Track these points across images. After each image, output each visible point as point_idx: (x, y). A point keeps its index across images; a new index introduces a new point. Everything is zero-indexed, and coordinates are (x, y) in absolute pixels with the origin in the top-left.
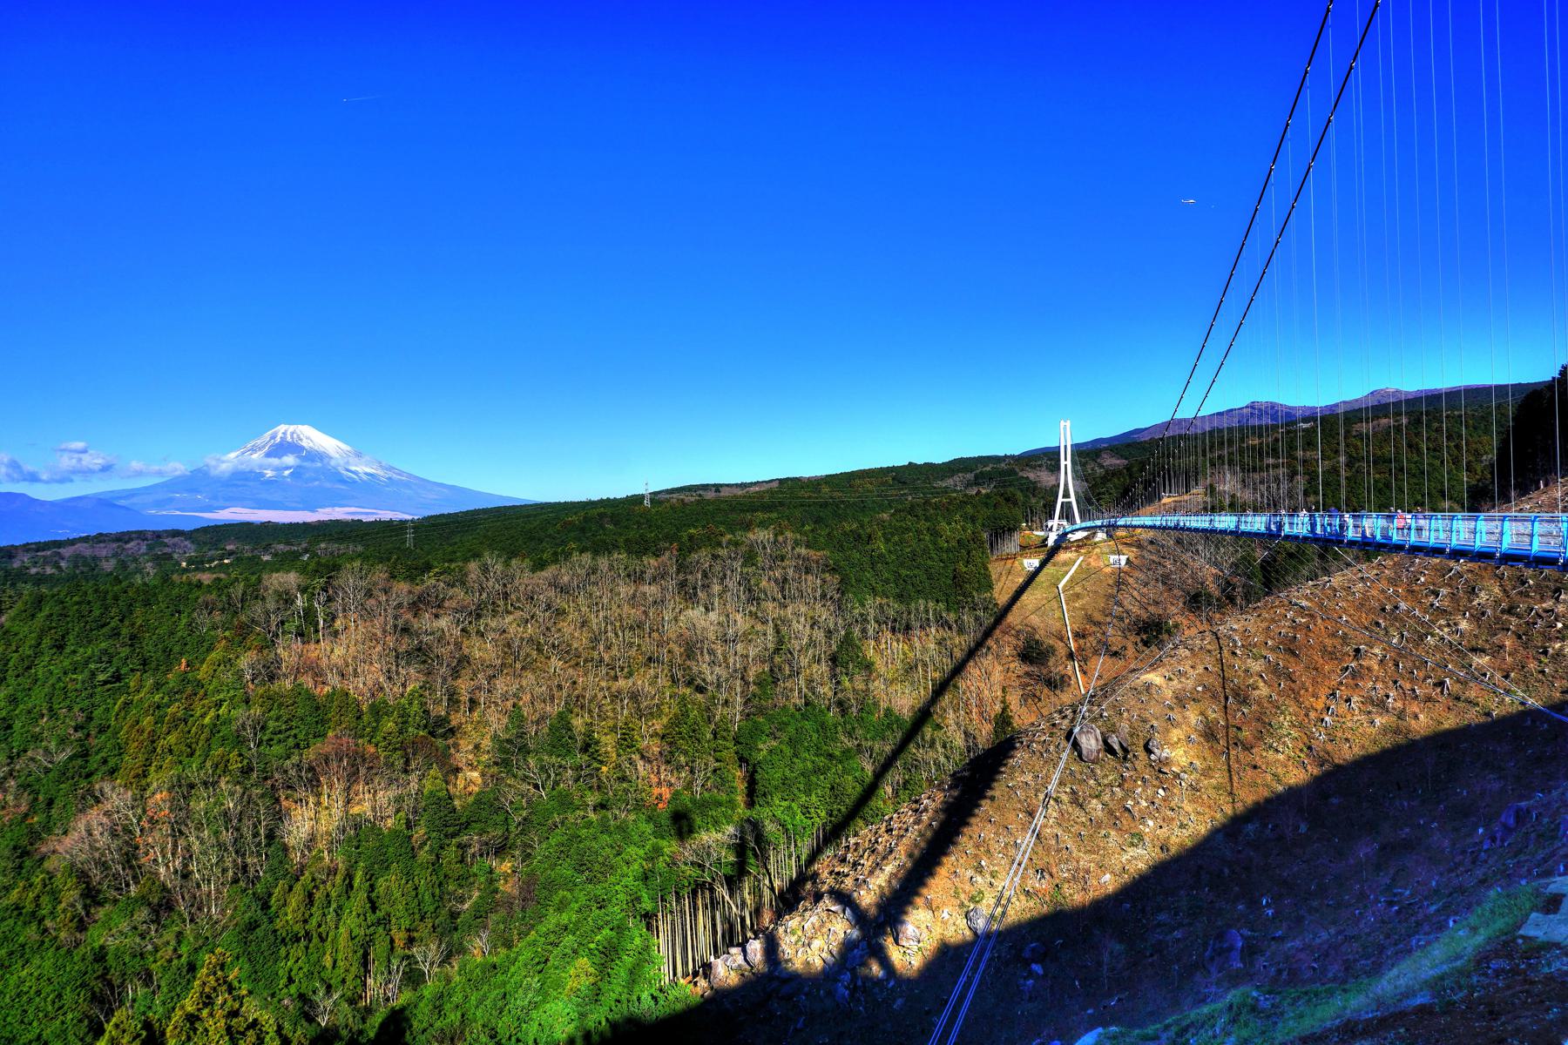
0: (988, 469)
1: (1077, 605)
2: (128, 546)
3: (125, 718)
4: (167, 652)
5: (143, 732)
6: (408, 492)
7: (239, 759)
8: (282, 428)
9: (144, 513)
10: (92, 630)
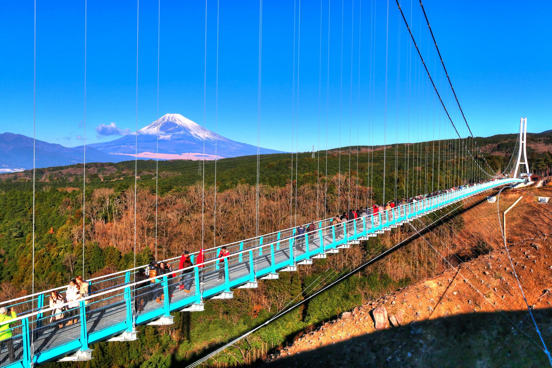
0: (506, 142)
1: (512, 224)
2: (90, 170)
3: (20, 254)
4: (46, 224)
5: (26, 261)
6: (223, 146)
7: (61, 277)
8: (168, 115)
9: (108, 154)
10: (16, 212)
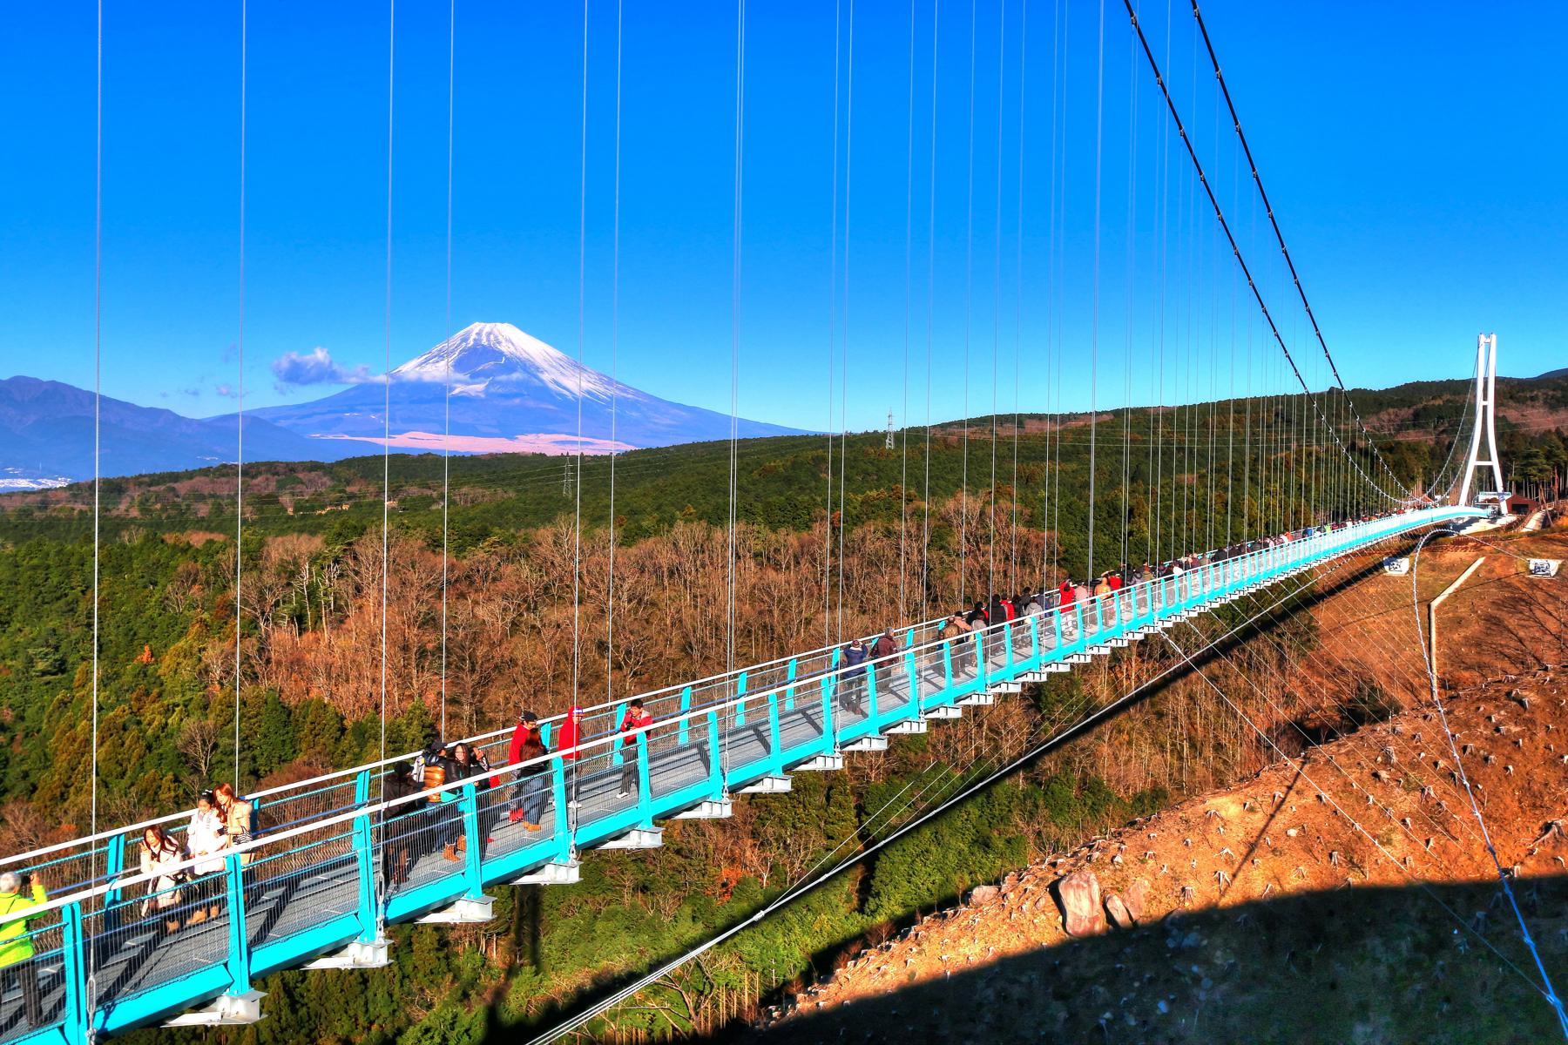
0: (1439, 402)
1: (1456, 636)
2: (255, 481)
3: (58, 722)
4: (131, 635)
5: (74, 740)
7: (172, 786)
8: (476, 328)
